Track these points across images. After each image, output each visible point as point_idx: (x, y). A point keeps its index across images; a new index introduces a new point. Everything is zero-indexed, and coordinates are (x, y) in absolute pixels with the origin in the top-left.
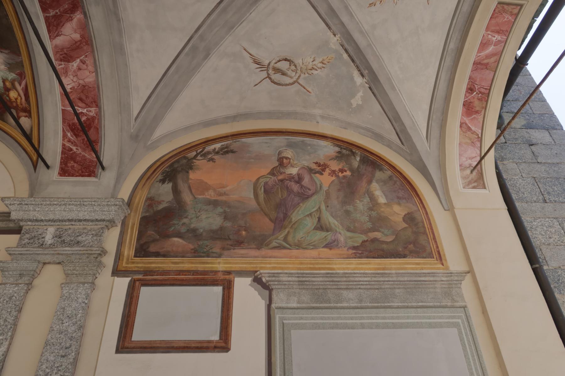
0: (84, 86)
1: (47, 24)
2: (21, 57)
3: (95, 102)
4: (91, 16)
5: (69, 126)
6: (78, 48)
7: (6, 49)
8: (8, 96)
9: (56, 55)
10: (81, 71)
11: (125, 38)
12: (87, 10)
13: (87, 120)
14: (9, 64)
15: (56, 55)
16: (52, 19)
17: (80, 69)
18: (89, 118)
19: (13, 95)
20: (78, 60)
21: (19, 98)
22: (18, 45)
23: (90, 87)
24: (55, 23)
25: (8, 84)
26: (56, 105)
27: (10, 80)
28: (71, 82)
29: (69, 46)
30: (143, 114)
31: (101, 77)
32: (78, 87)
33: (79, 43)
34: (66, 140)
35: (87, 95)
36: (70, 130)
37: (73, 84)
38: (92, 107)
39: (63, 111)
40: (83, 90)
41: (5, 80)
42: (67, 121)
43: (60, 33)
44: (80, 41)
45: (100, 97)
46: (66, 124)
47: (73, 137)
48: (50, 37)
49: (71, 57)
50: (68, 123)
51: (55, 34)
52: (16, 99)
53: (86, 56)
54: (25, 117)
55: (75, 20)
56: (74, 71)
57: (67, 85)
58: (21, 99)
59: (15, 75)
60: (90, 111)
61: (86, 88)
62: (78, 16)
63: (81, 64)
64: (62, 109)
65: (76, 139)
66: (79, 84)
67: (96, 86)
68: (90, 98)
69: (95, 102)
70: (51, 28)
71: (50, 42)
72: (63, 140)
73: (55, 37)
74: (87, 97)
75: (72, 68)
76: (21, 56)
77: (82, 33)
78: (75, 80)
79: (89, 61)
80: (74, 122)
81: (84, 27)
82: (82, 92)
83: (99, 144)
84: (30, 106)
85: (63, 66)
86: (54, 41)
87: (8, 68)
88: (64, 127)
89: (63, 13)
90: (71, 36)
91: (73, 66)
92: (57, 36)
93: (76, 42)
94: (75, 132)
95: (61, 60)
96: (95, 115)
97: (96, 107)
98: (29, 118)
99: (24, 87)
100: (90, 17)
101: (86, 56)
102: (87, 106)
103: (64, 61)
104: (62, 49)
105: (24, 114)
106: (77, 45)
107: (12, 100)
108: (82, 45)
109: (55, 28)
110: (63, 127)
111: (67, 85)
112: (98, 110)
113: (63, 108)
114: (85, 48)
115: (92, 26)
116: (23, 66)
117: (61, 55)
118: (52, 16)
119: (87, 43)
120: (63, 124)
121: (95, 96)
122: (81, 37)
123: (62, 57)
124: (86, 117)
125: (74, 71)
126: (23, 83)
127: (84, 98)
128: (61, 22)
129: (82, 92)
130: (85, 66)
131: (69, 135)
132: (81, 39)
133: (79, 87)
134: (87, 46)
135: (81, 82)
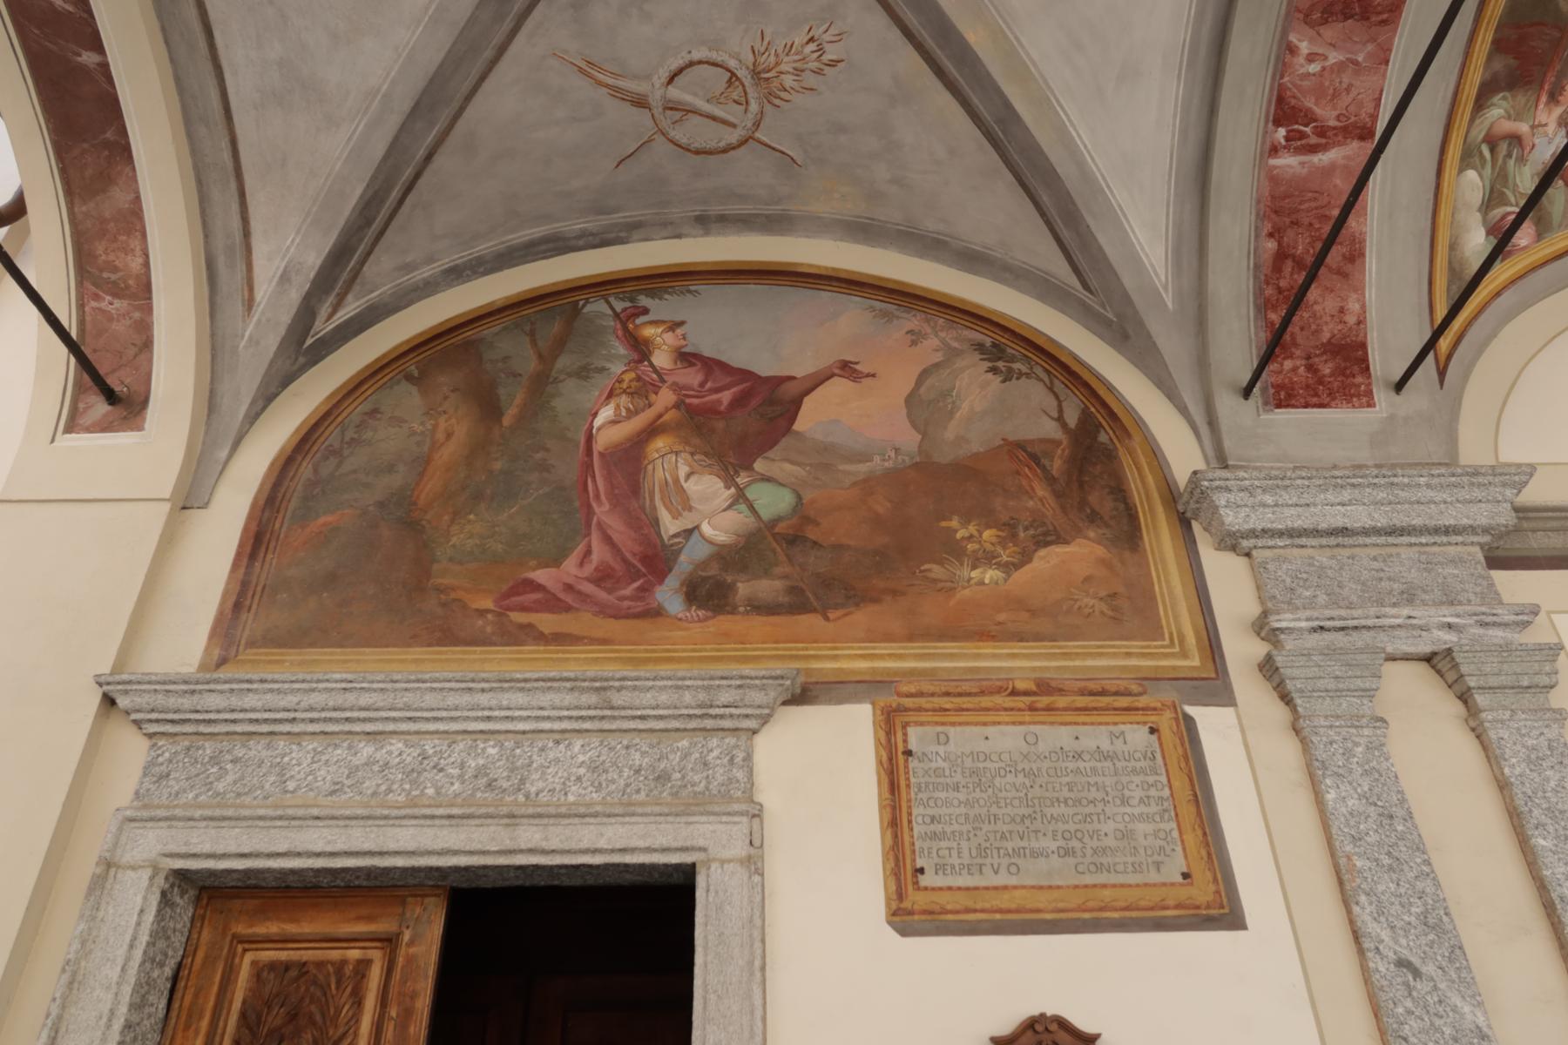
100: (623, 850)
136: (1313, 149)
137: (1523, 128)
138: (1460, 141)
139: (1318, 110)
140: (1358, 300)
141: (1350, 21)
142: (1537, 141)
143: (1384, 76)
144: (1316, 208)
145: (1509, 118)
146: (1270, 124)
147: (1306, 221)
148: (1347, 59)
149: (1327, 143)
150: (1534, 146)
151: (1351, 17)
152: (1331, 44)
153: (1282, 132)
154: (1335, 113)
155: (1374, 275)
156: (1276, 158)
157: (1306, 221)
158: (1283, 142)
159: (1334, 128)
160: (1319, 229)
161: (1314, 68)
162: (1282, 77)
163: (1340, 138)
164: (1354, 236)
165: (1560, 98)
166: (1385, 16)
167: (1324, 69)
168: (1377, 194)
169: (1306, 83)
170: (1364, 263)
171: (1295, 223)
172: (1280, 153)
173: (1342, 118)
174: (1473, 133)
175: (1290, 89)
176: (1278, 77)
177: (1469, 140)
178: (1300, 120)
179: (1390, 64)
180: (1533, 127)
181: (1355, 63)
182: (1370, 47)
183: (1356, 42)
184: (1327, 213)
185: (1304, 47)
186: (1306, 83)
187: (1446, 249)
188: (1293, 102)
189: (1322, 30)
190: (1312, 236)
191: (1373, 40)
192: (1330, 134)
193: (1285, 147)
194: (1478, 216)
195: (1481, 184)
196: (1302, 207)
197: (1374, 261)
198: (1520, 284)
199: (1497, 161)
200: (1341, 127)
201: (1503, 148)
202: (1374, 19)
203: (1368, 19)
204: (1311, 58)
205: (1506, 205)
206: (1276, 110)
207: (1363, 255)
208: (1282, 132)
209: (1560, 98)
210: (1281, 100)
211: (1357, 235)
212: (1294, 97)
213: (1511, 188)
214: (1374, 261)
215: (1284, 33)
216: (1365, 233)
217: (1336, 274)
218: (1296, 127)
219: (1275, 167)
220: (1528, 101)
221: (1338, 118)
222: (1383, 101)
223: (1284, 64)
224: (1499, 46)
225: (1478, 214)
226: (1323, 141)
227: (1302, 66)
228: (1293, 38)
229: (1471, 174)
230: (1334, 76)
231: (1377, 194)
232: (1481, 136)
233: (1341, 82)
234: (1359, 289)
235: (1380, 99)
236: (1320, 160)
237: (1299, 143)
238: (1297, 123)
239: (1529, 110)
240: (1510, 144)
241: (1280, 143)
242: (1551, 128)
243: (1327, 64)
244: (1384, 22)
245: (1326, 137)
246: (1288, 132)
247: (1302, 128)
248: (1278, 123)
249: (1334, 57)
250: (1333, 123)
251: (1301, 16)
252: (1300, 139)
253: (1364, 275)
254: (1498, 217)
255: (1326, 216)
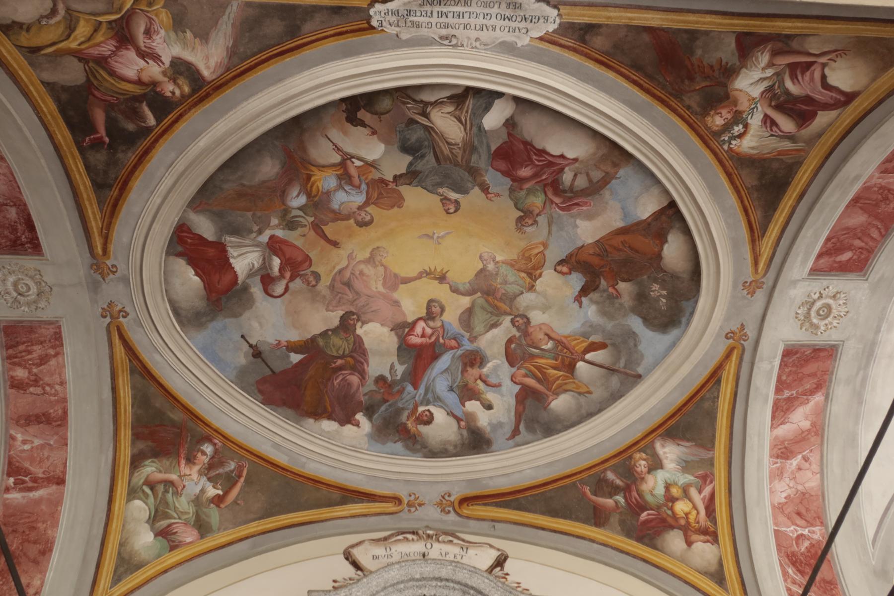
0: (804, 494)
1: (775, 408)
2: (712, 453)
3: (819, 518)
4: (834, 399)
5: (788, 556)
6: (804, 439)
7: (688, 440)
8: (671, 509)
9: (773, 449)
10: (801, 473)
11: (862, 425)
12: (831, 391)
13: (811, 547)
14: (685, 461)
15: (773, 449)
16: (783, 402)
17: (800, 469)
18: (813, 543)
19: (681, 507)
20: (800, 457)
21: (694, 513)
22: (714, 436)
23: (812, 496)
24: (785, 407)
25: (675, 491)
26: (767, 522)
27: (682, 485)
28: (787, 487)
29: (792, 438)
30: (882, 534)
31: (827, 481)
32: (795, 495)
33: (807, 433)
34: (789, 581)
35: (807, 506)
36: (790, 564)
37: (789, 491)
38: (816, 526)
39: (776, 532)
40: (802, 500)
41: (669, 485)
42: (783, 548)
43: (787, 421)
44: (809, 431)
45: (825, 511)
46: (782, 554)
47: (797, 576)
48: (772, 425)
49: (792, 452)
50: (785, 552)
51: (780, 422)
52: (687, 514)
53: (811, 451)
54: (705, 542)
55: (812, 403)
56: (792, 473)
57: (781, 492)
58: (698, 513)
59: (692, 478)
60: (814, 532)
61: (807, 496)
62: (819, 398)
63: (803, 462)
64: (774, 530)
65: (802, 578)
66: (797, 491)
67: (820, 493)
68: (812, 511)
69: (819, 518)
70: (777, 413)
71: (769, 432)
72: (785, 581)
73: (779, 425)
74: (808, 510)
75: (789, 468)
76: (714, 451)
77: (814, 420)
78: (791, 485)
79: (814, 458)
80: (793, 550)
81: (821, 413)
82: (801, 503)
83: (839, 587)
84: (715, 524)
85: (778, 465)
86: (776, 430)
87: (682, 467)
88: (781, 559)
89: (801, 395)
90: (799, 424)
91: (791, 464)
92: (781, 424)
93: (803, 432)
94: (797, 567)
95: (778, 457)
96: (821, 539)
97: (821, 526)
98: (713, 544)
99: (707, 496)
100: (832, 399)
101: (811, 451)
102: (809, 525)
103: (782, 458)
104: (783, 442)
105: (702, 537)
106: (803, 435)
107: (678, 515)
108: (809, 436)
109: (782, 413)
110: (779, 560)
111: (781, 492)
112: (824, 531)
113: (776, 528)
114: (812, 439)
115: (830, 411)
116: (712, 465)
117: (780, 449)
118: (785, 399)
119: (816, 434)
120: (778, 554)
121: (818, 508)
122: (811, 425)
123: (779, 451)
124: (809, 542)
125: (791, 472)
126: (707, 490)
127: (803, 511)
128: (793, 406)
129: (801, 503)
130: (807, 465)
131: (790, 571)
132: (811, 427)
133: (797, 495)
134: (815, 437)
135: (800, 487)
136: (30, 489)
137: (174, 477)
138: (126, 485)
139: (32, 469)
140: (41, 579)
141: (41, 425)
142: (186, 484)
143: (66, 452)
144: (29, 522)
145: (160, 472)
146: (5, 476)
147: (21, 530)
148: (45, 443)
149: (37, 487)
150: (184, 486)
151: (42, 423)
152: (34, 436)
153: (12, 480)
154: (42, 470)
155: (55, 563)
156: (8, 494)
157: (21, 530)
158: (12, 485)
159: (42, 478)
160: (28, 535)
161: (27, 447)
162: (10, 451)
163: (45, 483)
164: (49, 540)
165: (195, 461)
166: (59, 423)
167: (32, 448)
168: (66, 515)
169: (24, 455)
170: (51, 555)
171: (14, 531)
172: (11, 491)
173: (45, 473)
174: (135, 480)
175: (15, 458)
176: (7, 452)
177: (132, 484)
178: (22, 474)
179: (69, 446)
180: (180, 476)
181: (50, 445)
182: (56, 437)
183: (47, 435)
184: (35, 525)
185: (19, 437)
186: (24, 455)
187: (116, 546)
188: (17, 464)
189: (27, 428)
190: (23, 539)
191: (57, 434)
192: (40, 481)
193: (13, 488)
194: (147, 526)
195: (147, 508)
196: (21, 522)
197: (57, 554)
198: (187, 565)
199: (158, 495)
200: (46, 478)
201: (161, 488)
202: (54, 424)
203: (50, 424)
204: (24, 442)
205: (170, 518)
206: (8, 468)
207: (51, 550)
208: (12, 480)
209: (195, 461)
210: (10, 463)
211: (51, 538)
212: (18, 462)
213: (173, 508)
214: (57, 554)
215: (7, 430)
216: (56, 537)
217: (32, 562)
218: (20, 477)
219: (8, 499)
220: (171, 463)
221: (44, 473)
222: (68, 464)
223: (10, 446)
224: (137, 436)
225: (147, 525)
226: (36, 485)
227: (20, 446)
228: (12, 432)
229: (138, 503)
230: (39, 451)
231: (66, 515)
232: (142, 481)
233: (43, 455)
234: (43, 572)
235: (66, 463)
236: (34, 495)
237: (22, 486)
238: (20, 475)
239: (174, 467)
240: (165, 486)
241: (11, 486)
242: (195, 476)
243: (34, 445)
244: (59, 425)
245: (38, 482)
246: (15, 480)
247: (24, 478)
248: (9, 475)
249: (37, 442)
250: (41, 475)
251: (14, 422)
252: (22, 484)
253: (49, 563)
254: (165, 525)
255: (34, 527)
